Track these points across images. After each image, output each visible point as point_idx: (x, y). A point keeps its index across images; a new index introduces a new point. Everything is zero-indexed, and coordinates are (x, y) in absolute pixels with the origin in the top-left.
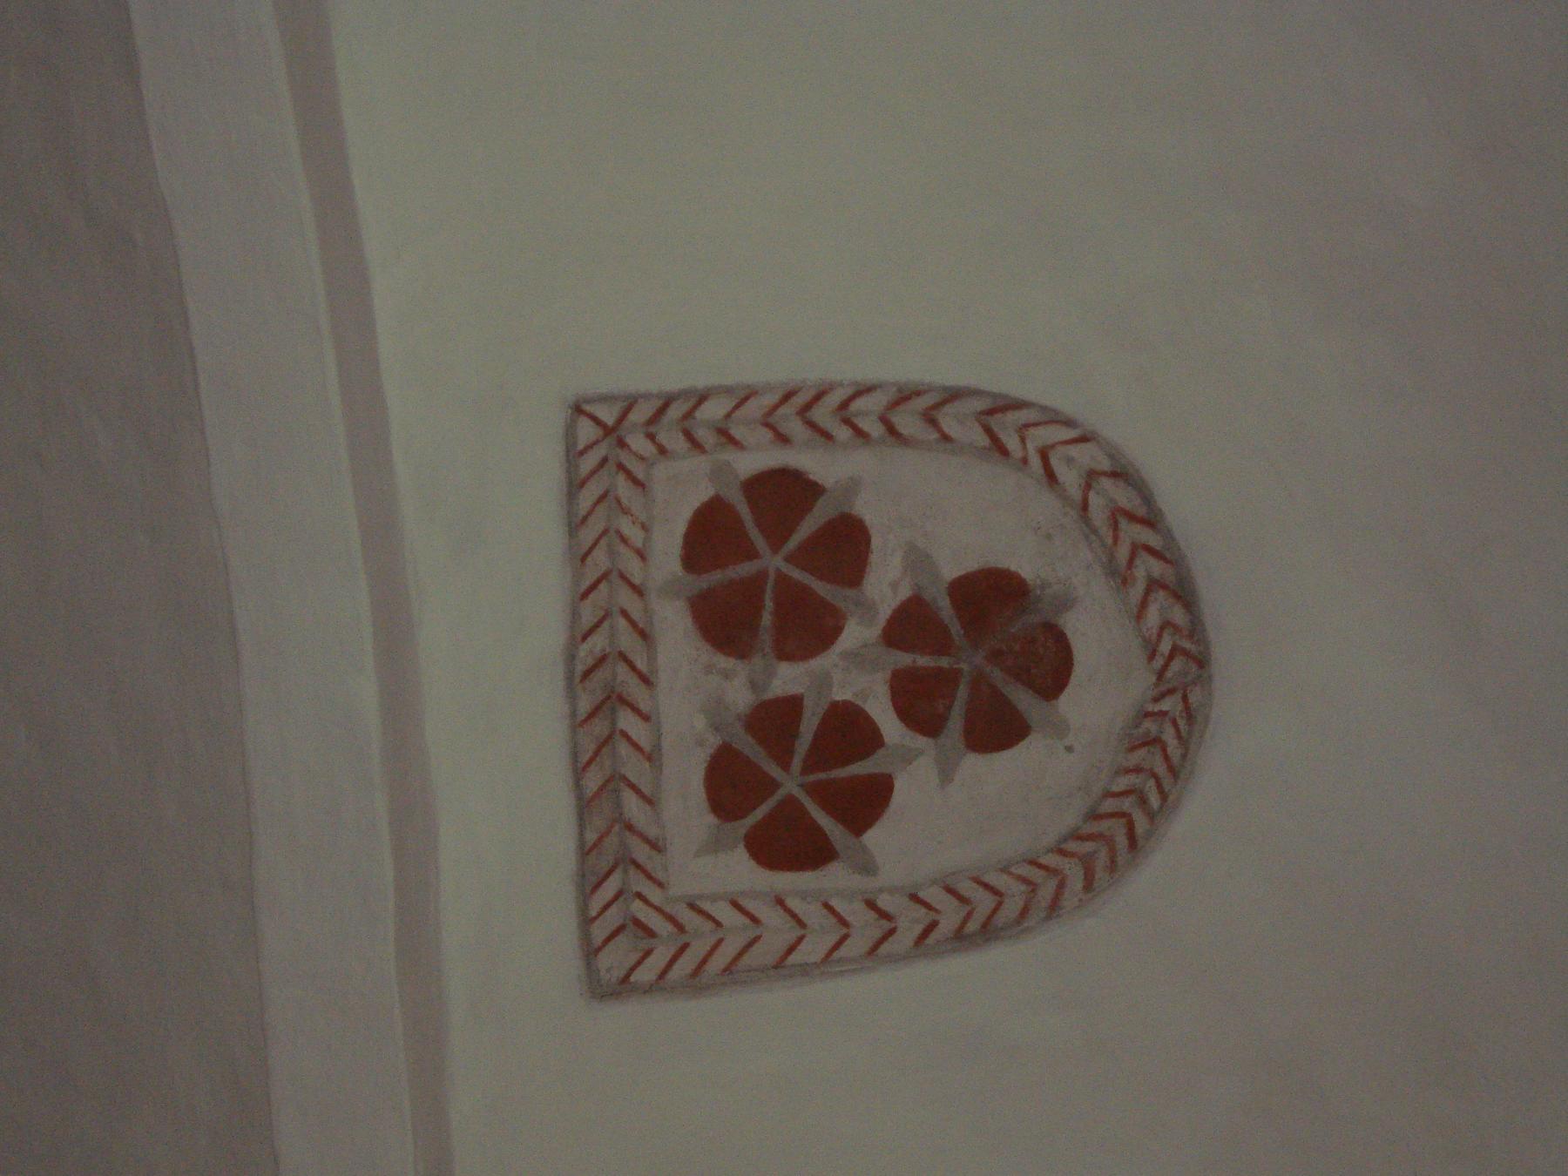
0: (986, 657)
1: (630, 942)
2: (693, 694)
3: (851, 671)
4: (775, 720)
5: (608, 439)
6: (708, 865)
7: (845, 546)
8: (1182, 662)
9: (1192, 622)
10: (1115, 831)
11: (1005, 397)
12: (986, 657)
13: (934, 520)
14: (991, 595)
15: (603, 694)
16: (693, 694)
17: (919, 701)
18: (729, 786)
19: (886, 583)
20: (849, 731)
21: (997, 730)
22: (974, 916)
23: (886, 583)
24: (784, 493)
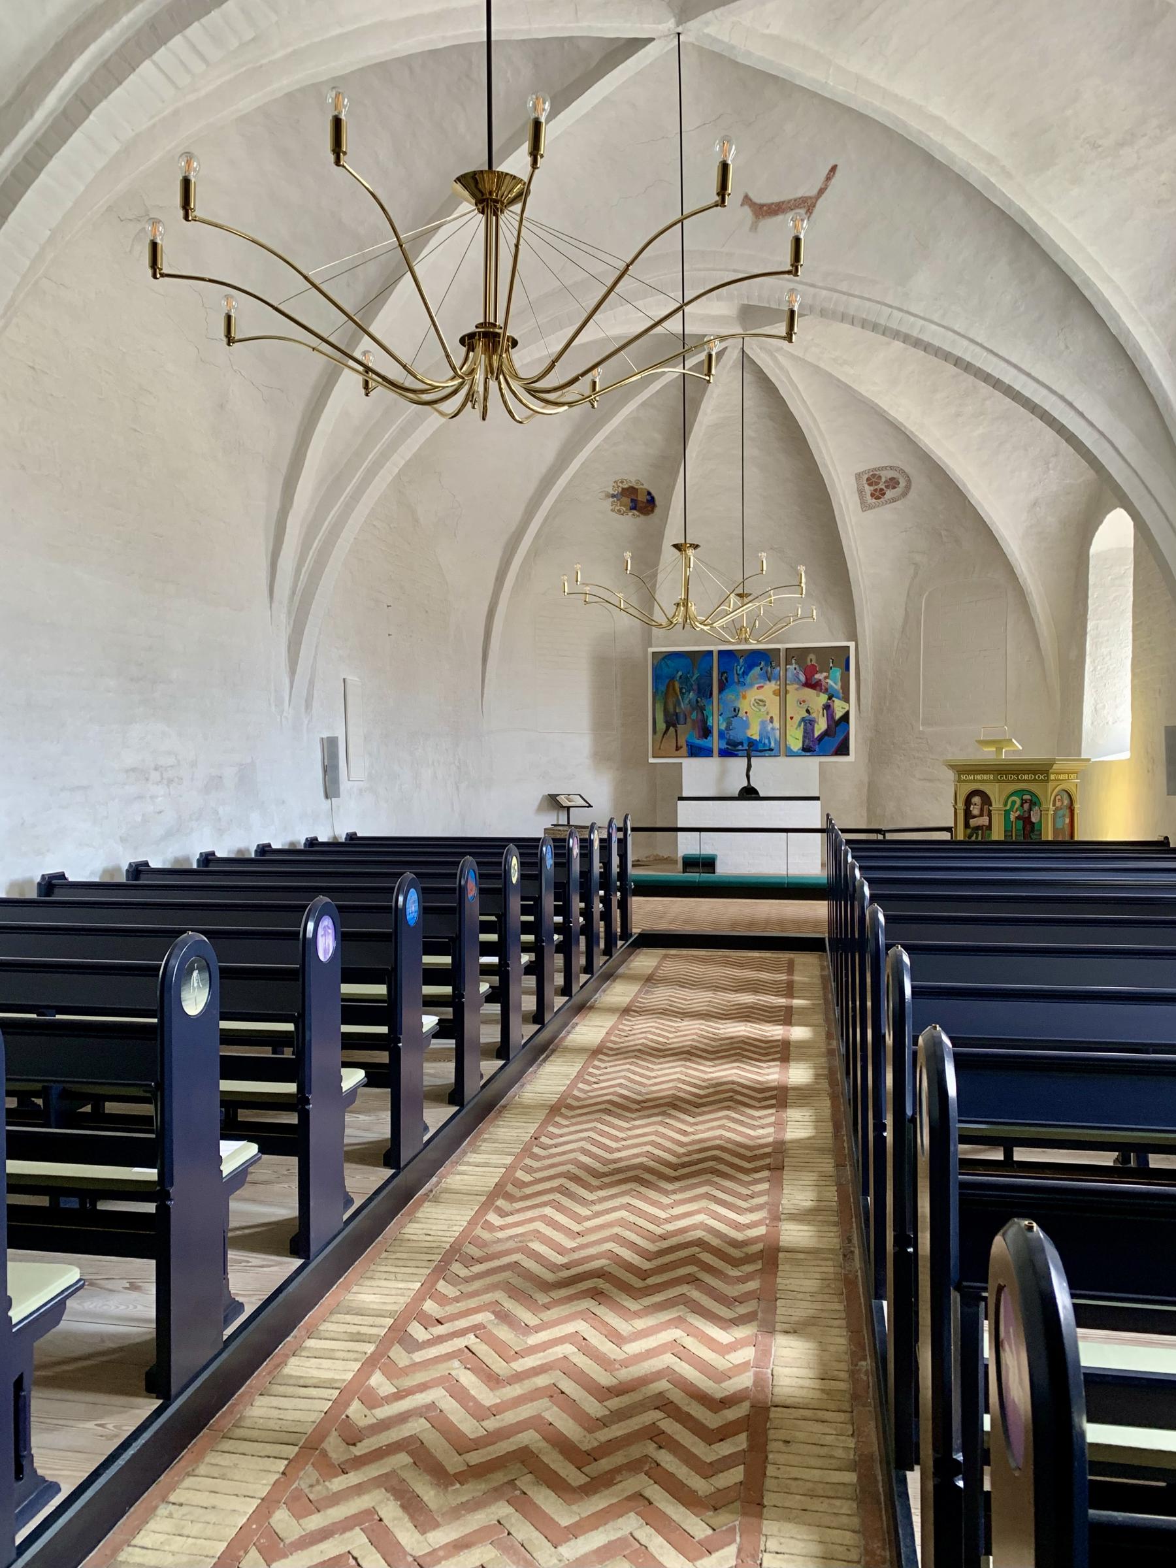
0: (893, 483)
1: (865, 507)
2: (868, 490)
3: (882, 486)
4: (876, 490)
5: (858, 476)
6: (870, 500)
7: (880, 477)
8: (909, 482)
9: (529, 1107)
10: (904, 494)
11: (690, 433)
12: (893, 483)
13: (886, 475)
14: (892, 479)
15: (861, 492)
16: (868, 490)
17: (887, 487)
18: (872, 495)
19: (883, 480)
20: (881, 490)
21: (894, 488)
22: (894, 500)
23: (883, 480)
24: (874, 475)
